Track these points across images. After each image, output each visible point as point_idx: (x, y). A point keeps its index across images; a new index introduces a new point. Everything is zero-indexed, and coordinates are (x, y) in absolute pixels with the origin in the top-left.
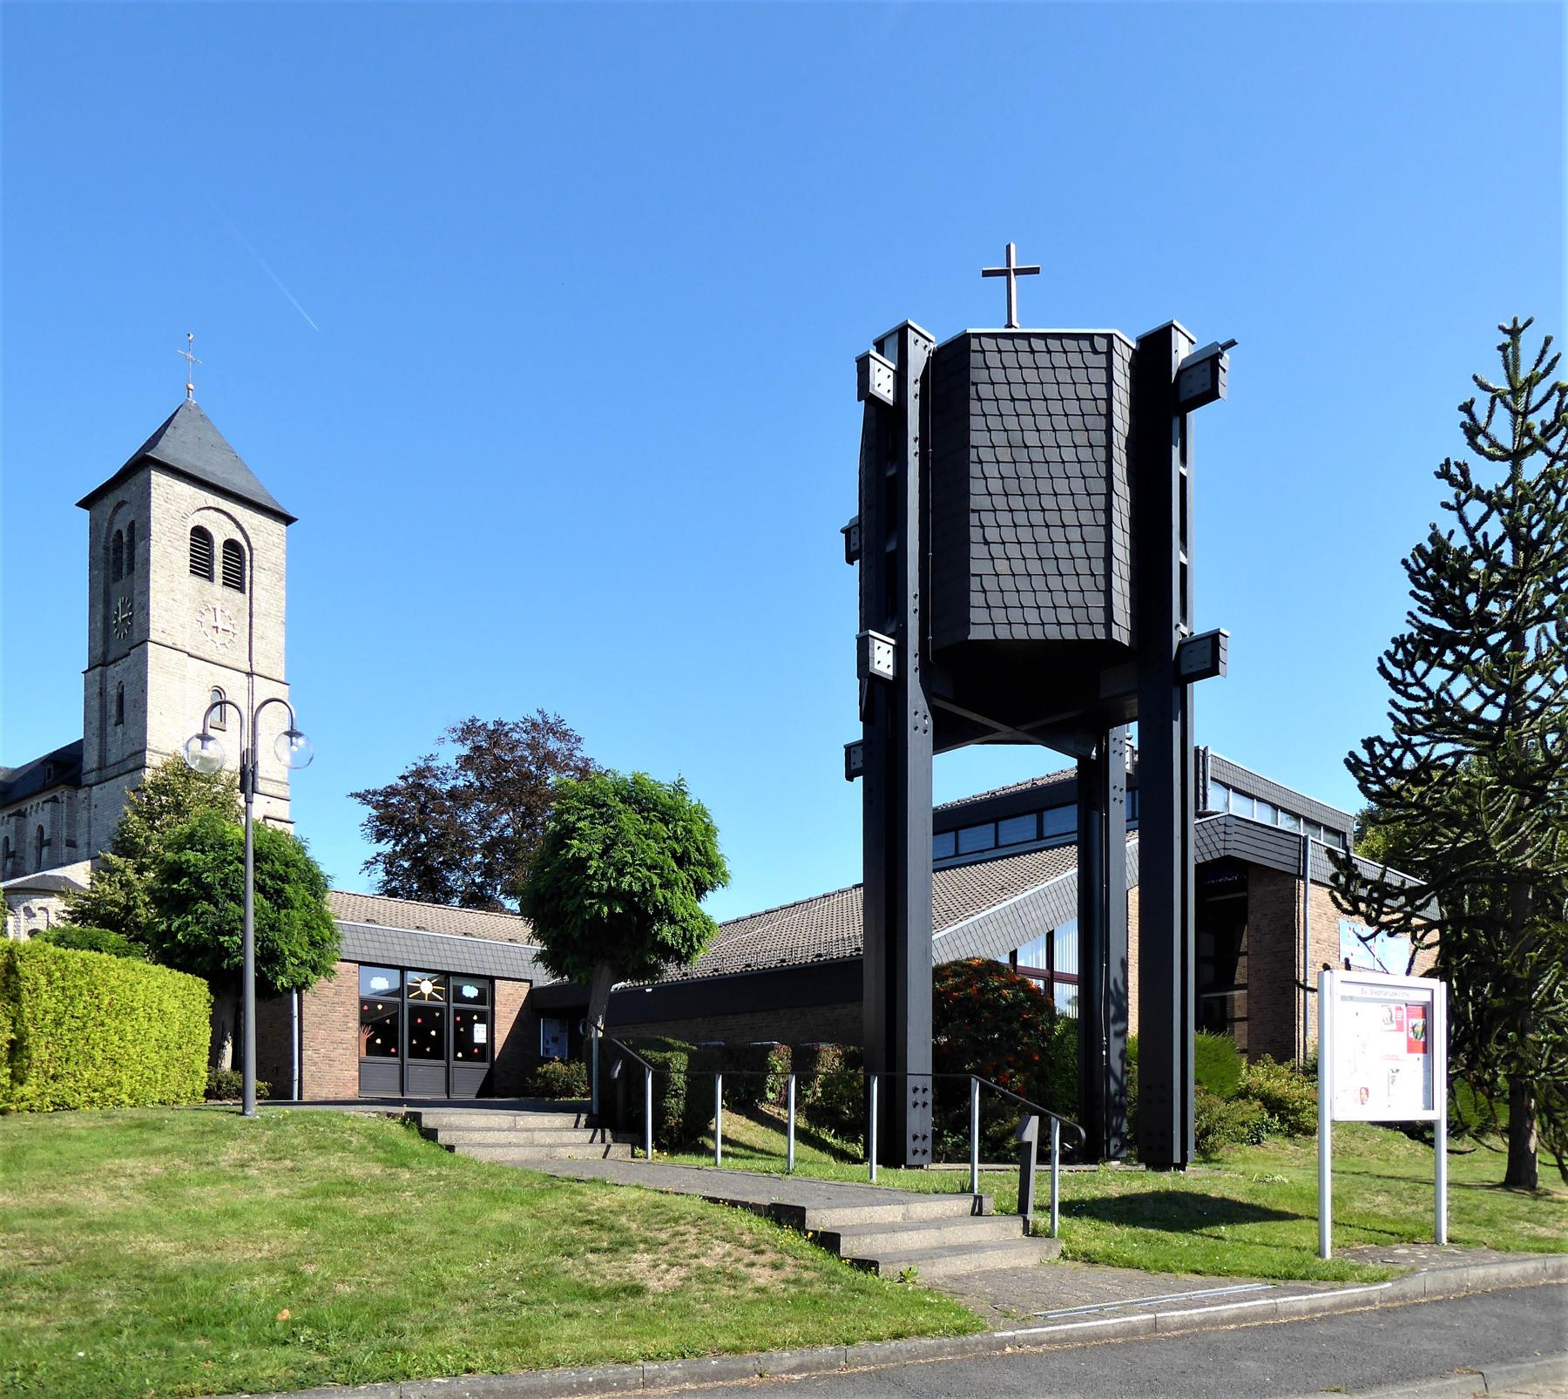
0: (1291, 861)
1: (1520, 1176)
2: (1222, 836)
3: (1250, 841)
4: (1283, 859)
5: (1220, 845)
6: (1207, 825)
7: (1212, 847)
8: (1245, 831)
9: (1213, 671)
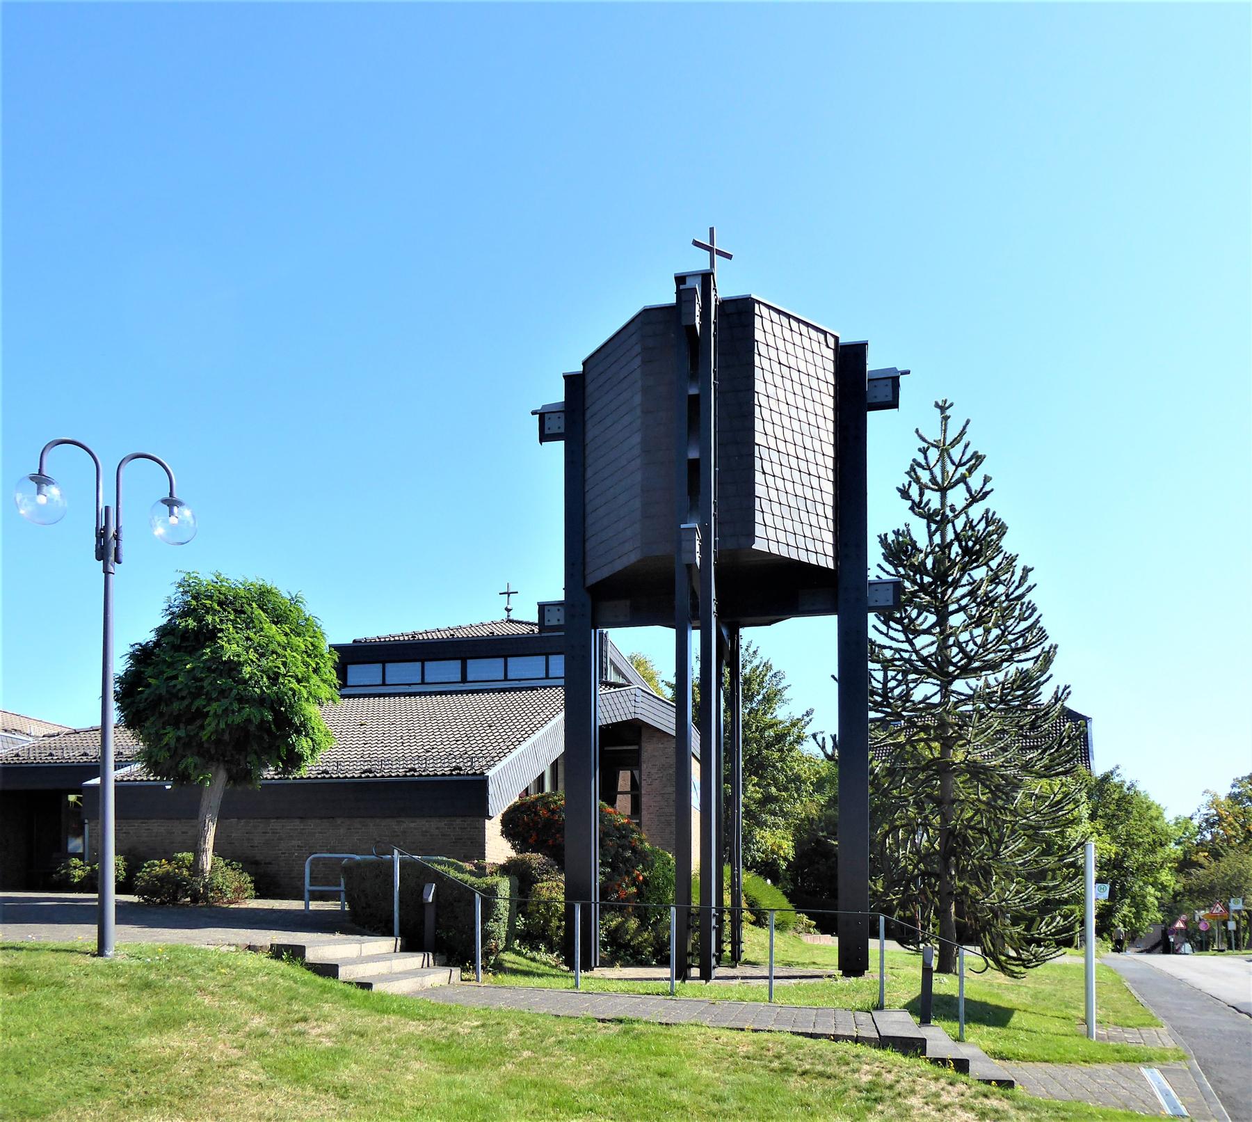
9: (893, 404)
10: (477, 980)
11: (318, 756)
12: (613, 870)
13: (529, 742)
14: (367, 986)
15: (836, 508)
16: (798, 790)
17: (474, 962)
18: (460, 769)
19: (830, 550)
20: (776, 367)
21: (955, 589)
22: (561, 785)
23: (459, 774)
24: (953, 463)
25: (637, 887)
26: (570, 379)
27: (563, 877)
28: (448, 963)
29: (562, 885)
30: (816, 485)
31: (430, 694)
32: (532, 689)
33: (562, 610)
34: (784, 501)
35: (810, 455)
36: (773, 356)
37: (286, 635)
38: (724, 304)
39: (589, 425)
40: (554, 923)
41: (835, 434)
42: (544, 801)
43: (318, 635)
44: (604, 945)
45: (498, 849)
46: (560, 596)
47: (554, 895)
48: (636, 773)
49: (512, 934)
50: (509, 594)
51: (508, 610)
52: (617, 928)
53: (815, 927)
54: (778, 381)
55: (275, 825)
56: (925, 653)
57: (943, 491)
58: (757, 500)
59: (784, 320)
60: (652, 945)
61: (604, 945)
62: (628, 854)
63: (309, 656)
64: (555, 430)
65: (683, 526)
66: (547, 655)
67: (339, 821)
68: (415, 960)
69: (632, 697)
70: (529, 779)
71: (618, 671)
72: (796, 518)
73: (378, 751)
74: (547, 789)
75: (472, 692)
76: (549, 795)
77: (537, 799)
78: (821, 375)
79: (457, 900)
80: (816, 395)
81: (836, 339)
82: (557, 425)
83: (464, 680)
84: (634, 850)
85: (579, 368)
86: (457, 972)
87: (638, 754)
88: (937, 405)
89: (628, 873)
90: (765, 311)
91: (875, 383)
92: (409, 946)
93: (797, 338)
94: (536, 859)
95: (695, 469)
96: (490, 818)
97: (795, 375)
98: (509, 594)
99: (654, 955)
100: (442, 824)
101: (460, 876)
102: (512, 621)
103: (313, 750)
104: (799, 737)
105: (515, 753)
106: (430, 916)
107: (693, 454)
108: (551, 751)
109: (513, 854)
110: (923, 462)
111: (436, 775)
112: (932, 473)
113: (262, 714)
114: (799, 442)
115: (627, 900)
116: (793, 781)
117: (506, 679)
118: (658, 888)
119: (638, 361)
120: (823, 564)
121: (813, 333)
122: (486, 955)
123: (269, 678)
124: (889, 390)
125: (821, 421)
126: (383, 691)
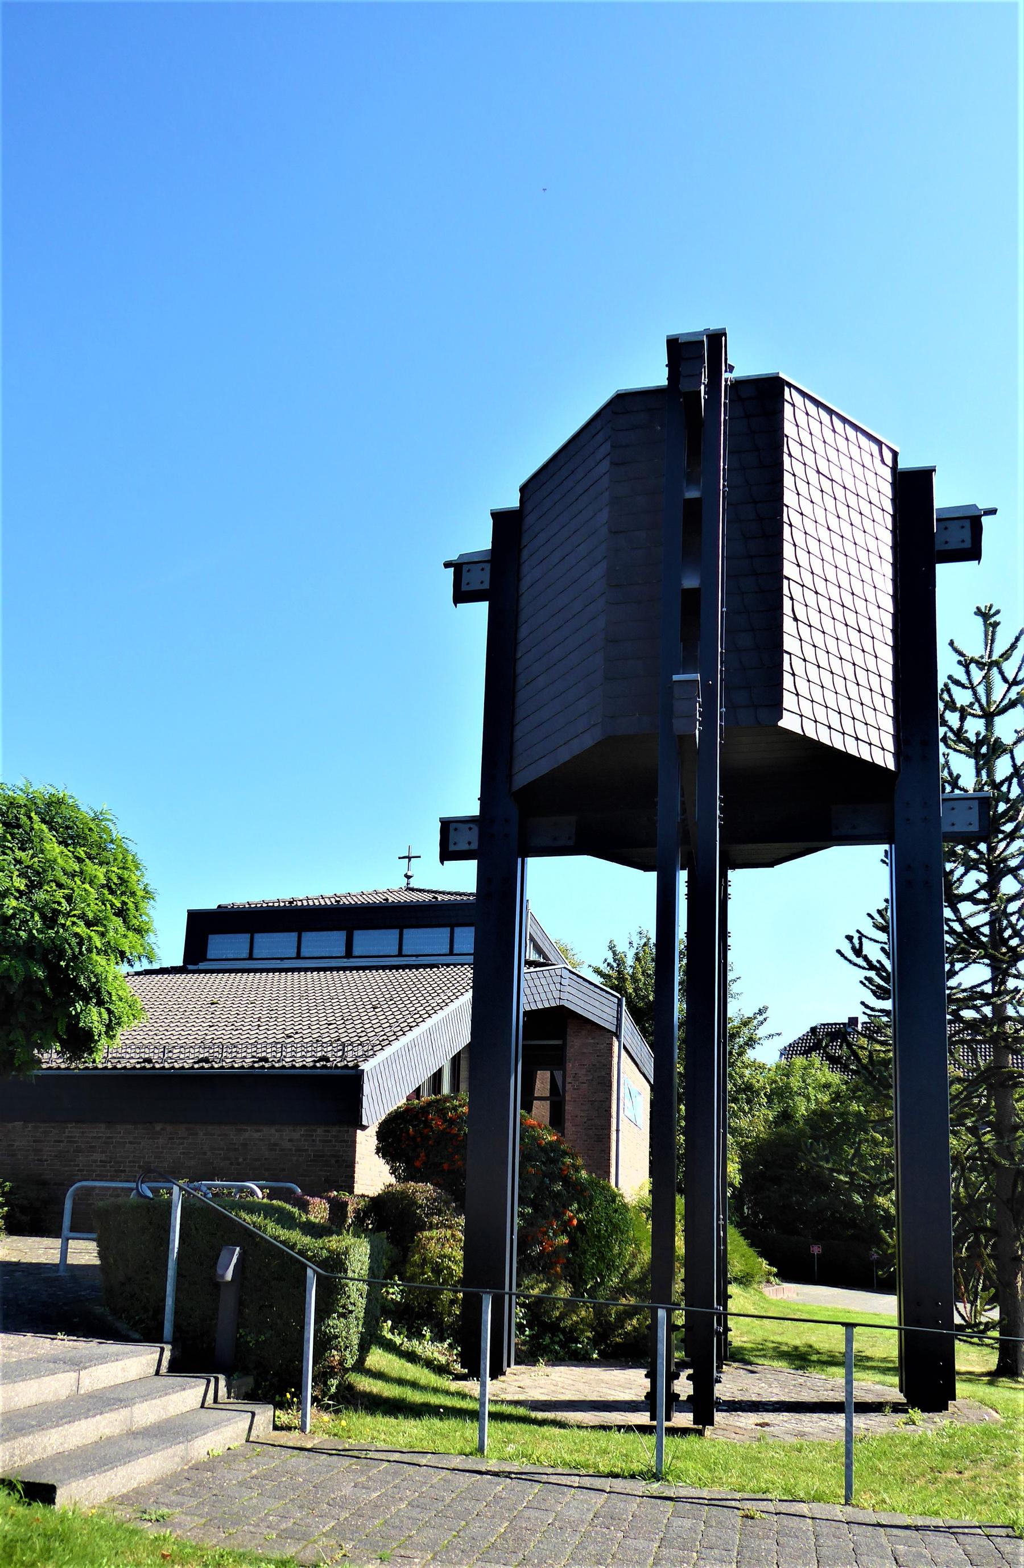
0: (610, 1019)
1: (927, 1380)
2: (558, 985)
3: (580, 995)
4: (605, 1016)
5: (556, 994)
6: (546, 974)
7: (550, 996)
8: (577, 986)
9: (973, 553)
10: (303, 1429)
11: (121, 1034)
12: (535, 1209)
13: (424, 1027)
14: (41, 1493)
15: (897, 683)
16: (749, 1101)
17: (299, 1393)
18: (327, 1060)
19: (889, 744)
20: (813, 477)
21: (1012, 840)
22: (464, 1086)
23: (324, 1067)
24: (1005, 680)
25: (569, 1235)
26: (500, 518)
27: (462, 1220)
28: (253, 1396)
29: (460, 1235)
30: (868, 648)
31: (306, 970)
32: (432, 966)
33: (476, 829)
34: (823, 663)
35: (860, 605)
36: (810, 461)
37: (80, 860)
38: (738, 385)
39: (525, 568)
40: (446, 1296)
41: (894, 581)
42: (438, 1106)
43: (130, 864)
44: (520, 1327)
45: (372, 1174)
46: (473, 809)
47: (448, 1250)
48: (558, 1074)
49: (378, 1310)
50: (409, 858)
51: (408, 877)
52: (539, 1301)
53: (776, 1275)
54: (816, 496)
55: (72, 1130)
56: (972, 923)
57: (989, 717)
58: (786, 657)
59: (825, 416)
60: (593, 1329)
61: (520, 1327)
62: (558, 1187)
63: (112, 892)
64: (475, 586)
65: (675, 678)
66: (452, 927)
67: (158, 1127)
68: (189, 1394)
69: (557, 979)
70: (422, 1076)
71: (539, 950)
72: (841, 690)
73: (225, 1034)
74: (446, 1089)
75: (358, 969)
76: (446, 1099)
77: (429, 1104)
78: (875, 497)
79: (276, 1276)
80: (868, 525)
81: (895, 454)
82: (481, 579)
83: (349, 954)
84: (566, 1181)
85: (512, 501)
86: (265, 1414)
87: (562, 1048)
88: (979, 612)
89: (558, 1215)
90: (798, 399)
91: (947, 524)
92: (183, 1365)
93: (842, 444)
94: (423, 1191)
95: (694, 605)
96: (364, 1128)
97: (839, 492)
98: (409, 858)
99: (595, 1342)
100: (296, 1135)
101: (284, 1234)
102: (413, 890)
103: (109, 1027)
104: (751, 1039)
105: (404, 1040)
106: (228, 1303)
107: (691, 582)
108: (451, 1040)
109: (393, 1180)
110: (964, 679)
111: (293, 1067)
112: (975, 693)
113: (27, 969)
114: (845, 584)
115: (555, 1252)
116: (744, 1091)
117: (400, 954)
118: (598, 1237)
119: (605, 466)
120: (879, 761)
121: (863, 441)
122: (321, 1378)
123: (43, 916)
124: (967, 534)
125: (875, 561)
126: (250, 964)
